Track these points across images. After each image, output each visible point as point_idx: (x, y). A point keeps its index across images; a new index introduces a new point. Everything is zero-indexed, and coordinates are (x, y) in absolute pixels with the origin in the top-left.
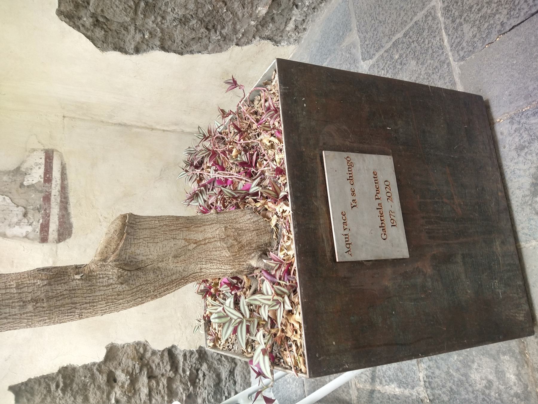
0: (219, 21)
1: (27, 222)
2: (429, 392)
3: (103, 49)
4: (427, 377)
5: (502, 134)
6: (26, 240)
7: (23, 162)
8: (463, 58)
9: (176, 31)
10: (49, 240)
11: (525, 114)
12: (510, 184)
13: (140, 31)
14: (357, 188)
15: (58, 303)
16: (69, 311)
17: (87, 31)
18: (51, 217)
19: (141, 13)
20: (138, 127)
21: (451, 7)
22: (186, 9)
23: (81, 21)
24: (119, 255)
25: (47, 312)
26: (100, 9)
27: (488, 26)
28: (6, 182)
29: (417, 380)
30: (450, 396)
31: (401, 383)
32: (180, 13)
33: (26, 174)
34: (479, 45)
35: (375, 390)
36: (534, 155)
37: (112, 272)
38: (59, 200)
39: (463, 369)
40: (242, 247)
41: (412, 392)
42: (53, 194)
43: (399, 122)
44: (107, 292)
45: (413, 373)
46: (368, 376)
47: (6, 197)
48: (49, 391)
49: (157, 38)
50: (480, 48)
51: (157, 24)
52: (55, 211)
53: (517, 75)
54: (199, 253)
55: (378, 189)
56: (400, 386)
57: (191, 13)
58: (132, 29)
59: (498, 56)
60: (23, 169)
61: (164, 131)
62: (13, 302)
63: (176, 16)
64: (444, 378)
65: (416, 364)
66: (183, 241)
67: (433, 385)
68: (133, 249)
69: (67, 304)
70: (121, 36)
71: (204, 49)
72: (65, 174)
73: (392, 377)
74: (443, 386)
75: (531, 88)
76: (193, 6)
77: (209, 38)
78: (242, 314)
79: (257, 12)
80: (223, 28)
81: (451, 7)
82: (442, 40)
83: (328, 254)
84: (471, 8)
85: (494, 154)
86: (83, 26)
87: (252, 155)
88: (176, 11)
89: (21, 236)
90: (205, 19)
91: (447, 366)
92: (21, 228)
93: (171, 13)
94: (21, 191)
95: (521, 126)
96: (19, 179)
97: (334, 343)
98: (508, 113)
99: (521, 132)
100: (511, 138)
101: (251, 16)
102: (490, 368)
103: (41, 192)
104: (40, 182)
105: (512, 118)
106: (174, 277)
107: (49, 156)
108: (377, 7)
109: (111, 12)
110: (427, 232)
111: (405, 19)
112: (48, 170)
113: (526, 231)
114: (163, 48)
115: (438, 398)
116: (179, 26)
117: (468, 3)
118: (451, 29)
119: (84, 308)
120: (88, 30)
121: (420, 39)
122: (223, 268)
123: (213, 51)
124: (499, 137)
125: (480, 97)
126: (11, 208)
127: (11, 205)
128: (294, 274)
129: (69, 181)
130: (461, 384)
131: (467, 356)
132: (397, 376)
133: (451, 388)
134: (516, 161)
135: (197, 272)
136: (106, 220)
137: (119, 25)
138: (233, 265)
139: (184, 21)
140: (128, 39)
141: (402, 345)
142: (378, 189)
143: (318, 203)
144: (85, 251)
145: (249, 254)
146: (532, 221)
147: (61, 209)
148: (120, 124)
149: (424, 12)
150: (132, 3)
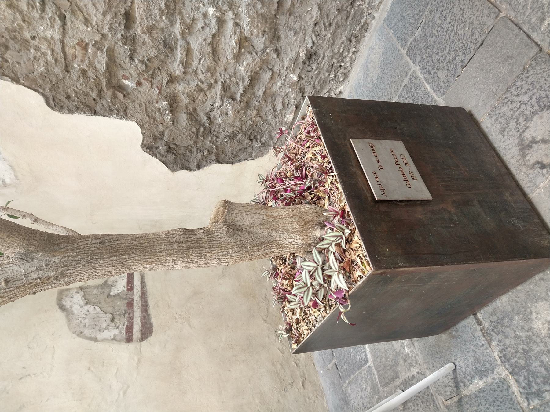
1: (114, 325)
2: (507, 366)
3: (173, 170)
4: (501, 351)
5: (487, 127)
6: (114, 342)
8: (444, 93)
9: (227, 146)
10: (133, 340)
11: (497, 107)
12: (505, 158)
13: (200, 151)
14: (380, 158)
15: (192, 245)
16: (198, 252)
17: (162, 157)
18: (134, 319)
19: (201, 136)
21: (425, 66)
23: (158, 150)
25: (186, 250)
26: (172, 138)
27: (454, 66)
28: (96, 294)
29: (494, 361)
30: (525, 357)
31: (481, 373)
32: (229, 131)
33: (112, 286)
34: (452, 80)
35: (462, 397)
36: (513, 130)
37: (222, 229)
39: (526, 326)
40: (306, 223)
41: (494, 376)
42: (135, 300)
43: (402, 124)
44: (221, 242)
45: (488, 357)
46: (452, 387)
47: (96, 307)
49: (213, 154)
50: (453, 82)
51: (213, 143)
52: (137, 314)
53: (482, 86)
54: (277, 224)
55: (396, 159)
56: (481, 377)
57: (237, 130)
58: (194, 150)
59: (466, 81)
60: (109, 282)
62: (165, 242)
63: (227, 134)
64: (515, 343)
65: (489, 346)
66: (265, 216)
67: (508, 357)
68: (233, 217)
69: (197, 247)
70: (186, 157)
71: (250, 156)
72: (144, 282)
73: (472, 373)
74: (516, 352)
75: (494, 90)
76: (238, 123)
77: (252, 147)
78: (316, 263)
79: (286, 119)
80: (262, 137)
81: (425, 66)
82: (426, 88)
83: (370, 198)
84: (438, 61)
85: (485, 141)
86: (159, 153)
87: (301, 172)
88: (227, 130)
89: (110, 339)
90: (248, 133)
91: (513, 331)
92: (110, 332)
93: (223, 132)
94: (109, 300)
95: (497, 116)
96: (106, 291)
97: (388, 250)
98: (486, 113)
99: (499, 120)
100: (494, 127)
101: (282, 123)
102: (546, 310)
103: (125, 299)
104: (123, 291)
105: (490, 114)
106: (262, 240)
108: (375, 89)
109: (180, 139)
110: (444, 187)
111: (396, 87)
113: (529, 184)
114: (218, 161)
115: (516, 367)
116: (229, 141)
117: (435, 59)
118: (430, 79)
119: (208, 252)
120: (162, 156)
121: (410, 95)
122: (295, 238)
123: (257, 157)
124: (486, 130)
125: (462, 109)
126: (101, 316)
127: (100, 313)
128: (348, 215)
129: (148, 288)
130: (530, 340)
131: (525, 311)
132: (476, 368)
133: (523, 349)
134: (503, 140)
135: (277, 240)
136: (181, 317)
137: (185, 149)
138: (302, 236)
139: (232, 137)
140: (192, 159)
141: (443, 255)
142: (396, 159)
143: (355, 169)
144: (165, 346)
145: (314, 227)
146: (530, 175)
147: (142, 312)
149: (409, 77)
150: (195, 129)
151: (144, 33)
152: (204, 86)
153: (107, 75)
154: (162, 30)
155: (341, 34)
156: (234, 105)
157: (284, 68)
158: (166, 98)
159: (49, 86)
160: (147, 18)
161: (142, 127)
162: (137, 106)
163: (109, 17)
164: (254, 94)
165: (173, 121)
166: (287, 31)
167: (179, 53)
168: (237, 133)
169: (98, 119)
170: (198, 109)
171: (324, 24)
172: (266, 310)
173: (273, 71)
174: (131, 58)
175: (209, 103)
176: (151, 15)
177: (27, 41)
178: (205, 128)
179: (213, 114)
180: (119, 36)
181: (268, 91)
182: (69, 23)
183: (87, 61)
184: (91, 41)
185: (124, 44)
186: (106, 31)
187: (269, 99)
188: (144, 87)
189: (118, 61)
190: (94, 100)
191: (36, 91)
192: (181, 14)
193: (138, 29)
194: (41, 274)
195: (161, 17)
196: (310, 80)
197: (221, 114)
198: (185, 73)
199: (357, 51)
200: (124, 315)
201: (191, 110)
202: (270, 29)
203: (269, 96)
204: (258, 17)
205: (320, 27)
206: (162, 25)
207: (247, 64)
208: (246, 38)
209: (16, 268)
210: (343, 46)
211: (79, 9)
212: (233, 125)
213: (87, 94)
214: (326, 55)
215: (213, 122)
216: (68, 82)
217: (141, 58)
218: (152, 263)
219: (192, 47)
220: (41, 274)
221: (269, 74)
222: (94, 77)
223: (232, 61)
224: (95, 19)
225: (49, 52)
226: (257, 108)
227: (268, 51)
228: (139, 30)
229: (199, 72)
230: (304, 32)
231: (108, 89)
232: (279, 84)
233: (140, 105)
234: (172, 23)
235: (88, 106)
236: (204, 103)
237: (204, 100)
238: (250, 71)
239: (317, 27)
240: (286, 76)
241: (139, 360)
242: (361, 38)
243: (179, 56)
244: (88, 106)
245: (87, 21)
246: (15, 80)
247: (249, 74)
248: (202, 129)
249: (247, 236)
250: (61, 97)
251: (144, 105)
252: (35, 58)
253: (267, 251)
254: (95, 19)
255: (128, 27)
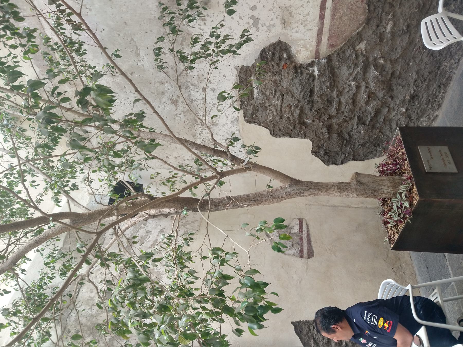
0: (380, 142)
3: (327, 165)
7: (290, 224)
20: (341, 207)
22: (364, 139)
24: (356, 179)
32: (362, 142)
37: (355, 183)
38: (307, 240)
48: (310, 330)
51: (351, 149)
58: (340, 153)
61: (356, 208)
63: (360, 143)
70: (335, 157)
103: (299, 236)
106: (373, 189)
107: (301, 221)
112: (301, 227)
114: (354, 159)
129: (311, 232)
139: (363, 145)
144: (321, 264)
147: (308, 244)
148: (332, 206)
151: (318, 98)
152: (348, 119)
153: (299, 118)
154: (327, 95)
155: (433, 84)
156: (365, 127)
157: (396, 105)
158: (326, 127)
159: (273, 125)
160: (320, 91)
161: (313, 142)
162: (311, 132)
163: (303, 93)
164: (377, 120)
165: (329, 138)
166: (398, 86)
167: (335, 105)
168: (366, 142)
169: (292, 139)
170: (343, 131)
171: (421, 80)
172: (386, 255)
173: (389, 108)
174: (311, 110)
175: (350, 128)
176: (322, 90)
177: (266, 107)
178: (347, 141)
179: (352, 133)
180: (306, 100)
181: (386, 118)
182: (285, 98)
183: (290, 113)
184: (293, 104)
185: (308, 104)
186: (301, 99)
187: (387, 123)
188: (316, 122)
189: (304, 111)
190: (291, 130)
191: (267, 128)
192: (337, 87)
193: (315, 97)
194: (294, 191)
195: (327, 90)
196: (414, 110)
197: (357, 132)
198: (337, 113)
199: (446, 92)
200: (298, 244)
201: (339, 132)
202: (387, 87)
203: (387, 121)
204: (379, 82)
205: (418, 82)
206: (327, 93)
207: (373, 106)
208: (373, 93)
209: (288, 189)
210: (435, 90)
211: (290, 91)
212: (364, 139)
213: (288, 128)
214: (424, 95)
215: (352, 138)
216: (281, 123)
217: (315, 109)
218: (328, 192)
219: (342, 101)
220: (294, 191)
221: (387, 109)
222: (293, 120)
223: (364, 105)
224: (296, 95)
225: (275, 111)
226: (379, 128)
227: (386, 97)
228: (316, 97)
229: (345, 112)
230: (408, 86)
231: (298, 125)
232: (393, 114)
233: (313, 131)
234: (332, 91)
235: (288, 133)
236: (346, 127)
237: (347, 126)
238: (374, 109)
239: (416, 82)
240: (398, 109)
241: (307, 268)
242: (447, 85)
243: (335, 106)
244: (288, 133)
245: (293, 96)
246: (259, 124)
247: (374, 110)
248: (345, 141)
249: (366, 186)
250: (277, 130)
251: (315, 131)
252: (269, 114)
253: (375, 194)
254: (296, 95)
255: (310, 96)
